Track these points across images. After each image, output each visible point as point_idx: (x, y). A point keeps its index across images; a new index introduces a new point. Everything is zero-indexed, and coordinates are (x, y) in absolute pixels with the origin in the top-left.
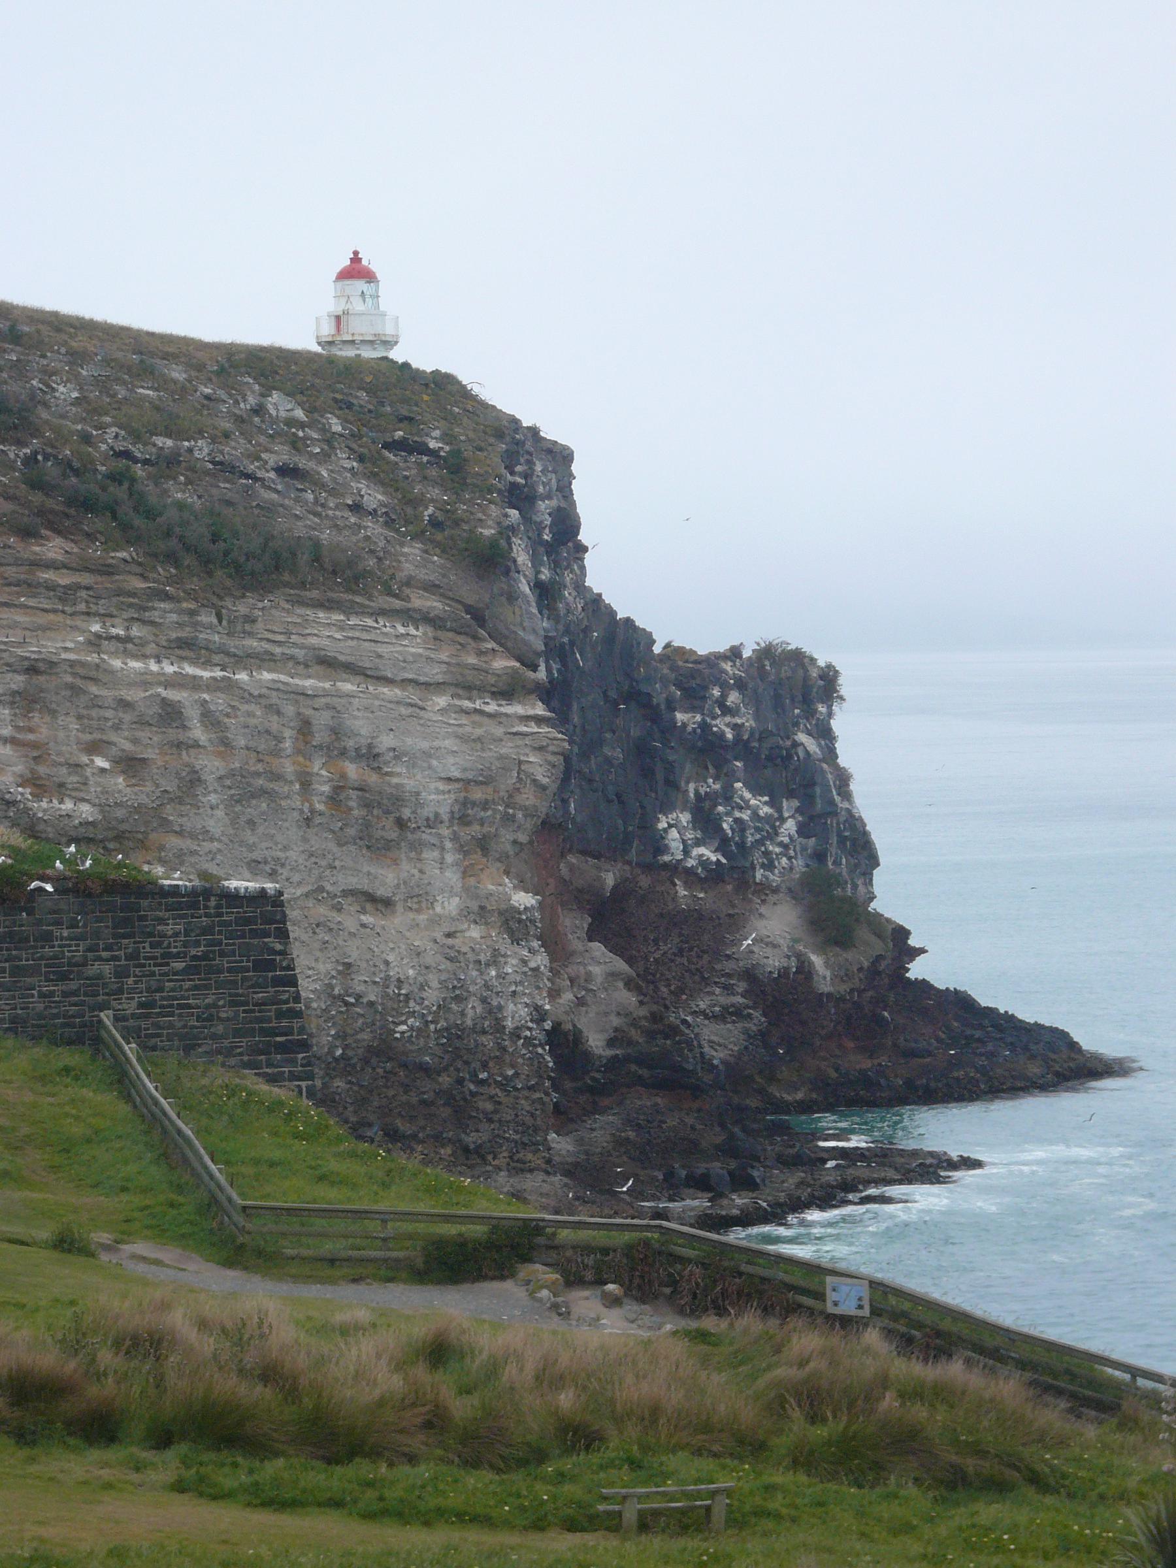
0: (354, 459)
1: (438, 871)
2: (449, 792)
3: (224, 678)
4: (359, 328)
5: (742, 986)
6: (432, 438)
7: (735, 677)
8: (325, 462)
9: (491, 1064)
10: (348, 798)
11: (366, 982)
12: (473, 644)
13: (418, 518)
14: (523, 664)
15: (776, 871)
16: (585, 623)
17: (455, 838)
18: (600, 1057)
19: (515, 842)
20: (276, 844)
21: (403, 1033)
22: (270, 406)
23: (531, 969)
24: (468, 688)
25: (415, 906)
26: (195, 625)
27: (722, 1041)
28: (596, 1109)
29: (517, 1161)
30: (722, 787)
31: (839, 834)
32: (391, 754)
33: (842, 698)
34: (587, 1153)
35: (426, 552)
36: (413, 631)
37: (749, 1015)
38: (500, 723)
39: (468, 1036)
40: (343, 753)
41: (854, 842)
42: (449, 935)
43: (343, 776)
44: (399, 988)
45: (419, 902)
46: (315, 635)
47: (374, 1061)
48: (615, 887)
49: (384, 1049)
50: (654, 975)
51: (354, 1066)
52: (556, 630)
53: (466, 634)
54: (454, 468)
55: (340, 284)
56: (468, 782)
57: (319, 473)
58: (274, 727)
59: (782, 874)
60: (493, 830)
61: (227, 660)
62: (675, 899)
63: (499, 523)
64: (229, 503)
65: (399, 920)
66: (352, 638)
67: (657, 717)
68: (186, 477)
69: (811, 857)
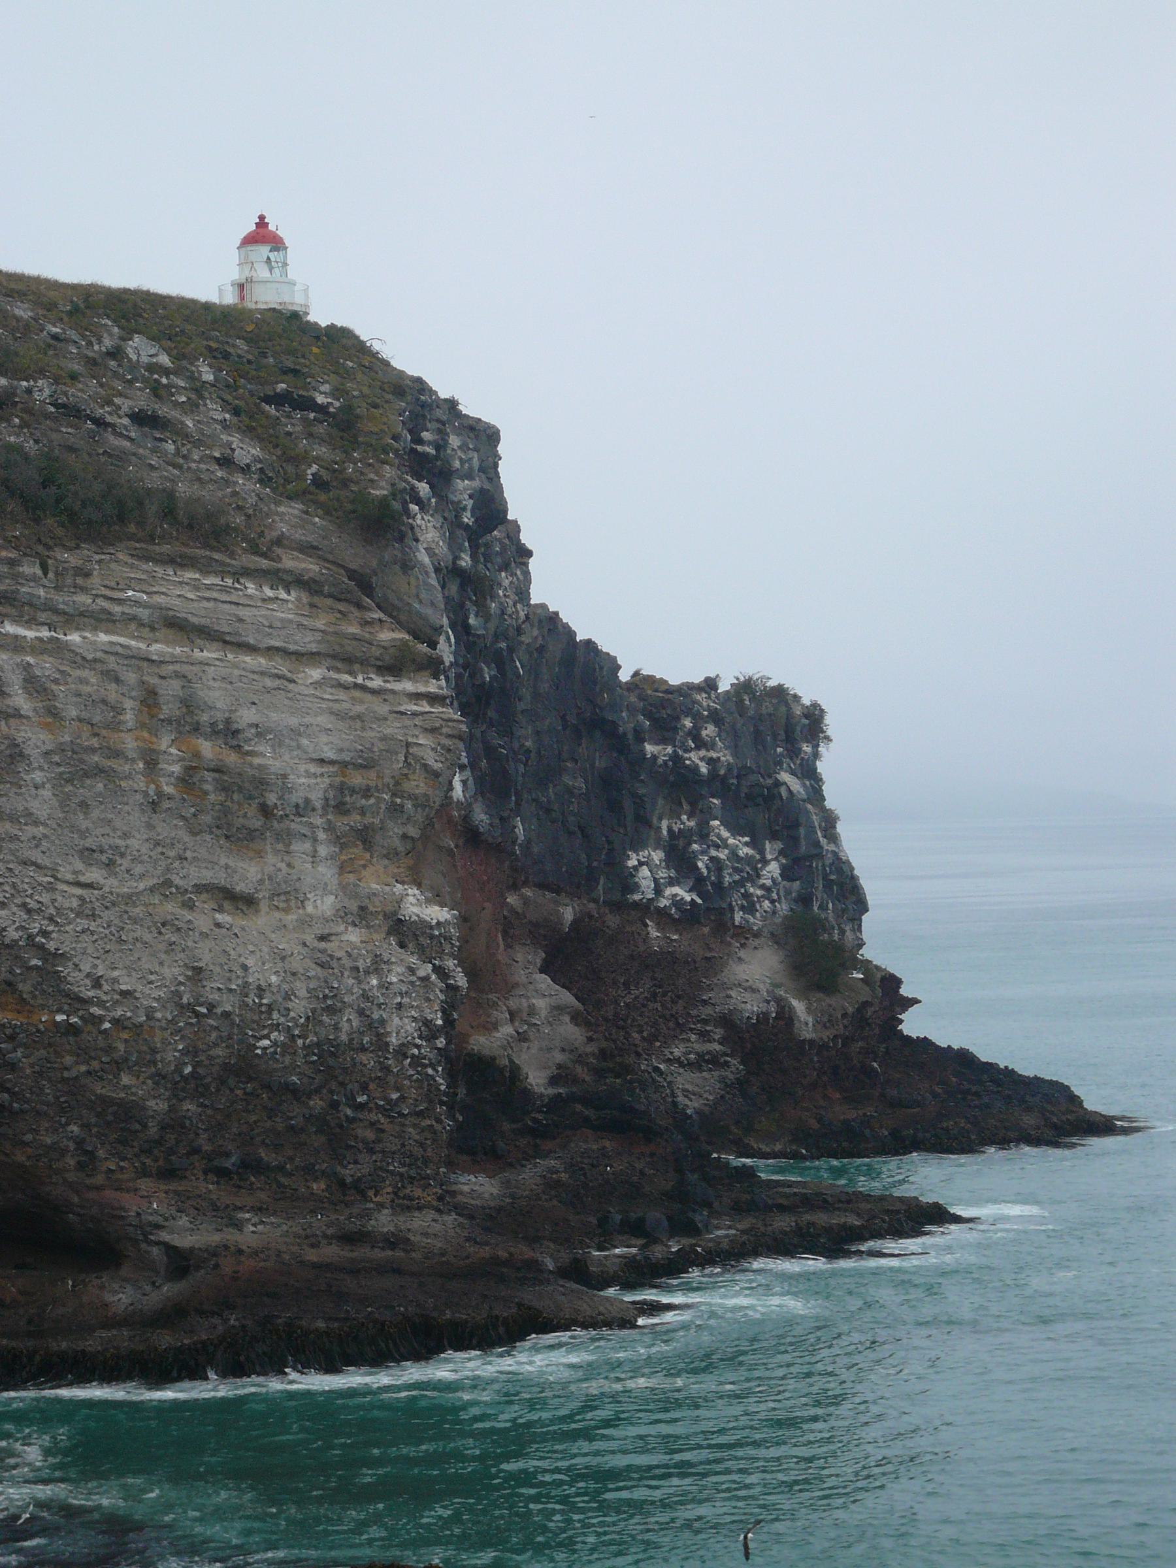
0: (228, 412)
1: (309, 866)
2: (322, 775)
3: (51, 639)
4: (265, 297)
5: (719, 1033)
6: (321, 393)
7: (709, 708)
8: (192, 412)
9: (372, 1086)
10: (203, 780)
11: (219, 989)
12: (357, 614)
13: (300, 477)
14: (416, 637)
15: (758, 914)
16: (540, 641)
17: (330, 828)
18: (542, 1095)
19: (405, 837)
20: (114, 830)
21: (265, 1049)
22: (130, 351)
23: (420, 978)
24: (348, 661)
25: (282, 905)
26: (16, 577)
27: (696, 1089)
28: (539, 1153)
29: (404, 1198)
30: (697, 824)
31: (825, 878)
32: (253, 731)
33: (828, 739)
34: (513, 1196)
35: (306, 513)
36: (283, 595)
37: (726, 1064)
38: (385, 700)
39: (344, 1053)
40: (196, 729)
41: (841, 886)
42: (322, 938)
43: (197, 755)
44: (261, 997)
45: (287, 901)
46: (163, 593)
47: (231, 1082)
48: (575, 922)
49: (244, 1067)
50: (625, 1021)
51: (206, 1087)
52: (485, 629)
53: (346, 600)
54: (345, 426)
56: (344, 765)
57: (182, 423)
58: (112, 697)
59: (764, 919)
60: (377, 821)
61: (55, 618)
62: (646, 939)
63: (393, 485)
64: (71, 449)
65: (263, 920)
66: (208, 599)
67: (622, 746)
68: (21, 419)
69: (796, 901)
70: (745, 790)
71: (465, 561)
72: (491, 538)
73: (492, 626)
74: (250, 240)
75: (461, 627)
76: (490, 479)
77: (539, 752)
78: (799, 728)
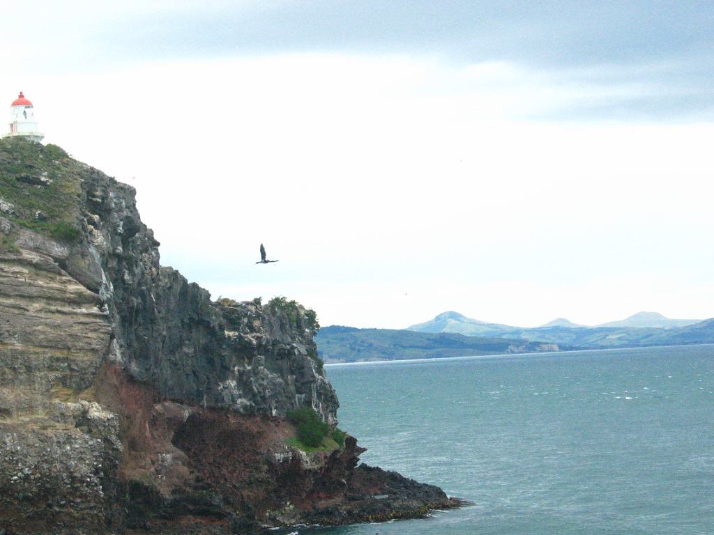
4: (22, 131)
6: (43, 176)
16: (169, 284)
21: (15, 480)
55: (13, 108)
70: (276, 352)
71: (120, 249)
72: (135, 239)
73: (136, 280)
74: (16, 104)
75: (118, 281)
76: (131, 212)
77: (170, 338)
78: (303, 321)
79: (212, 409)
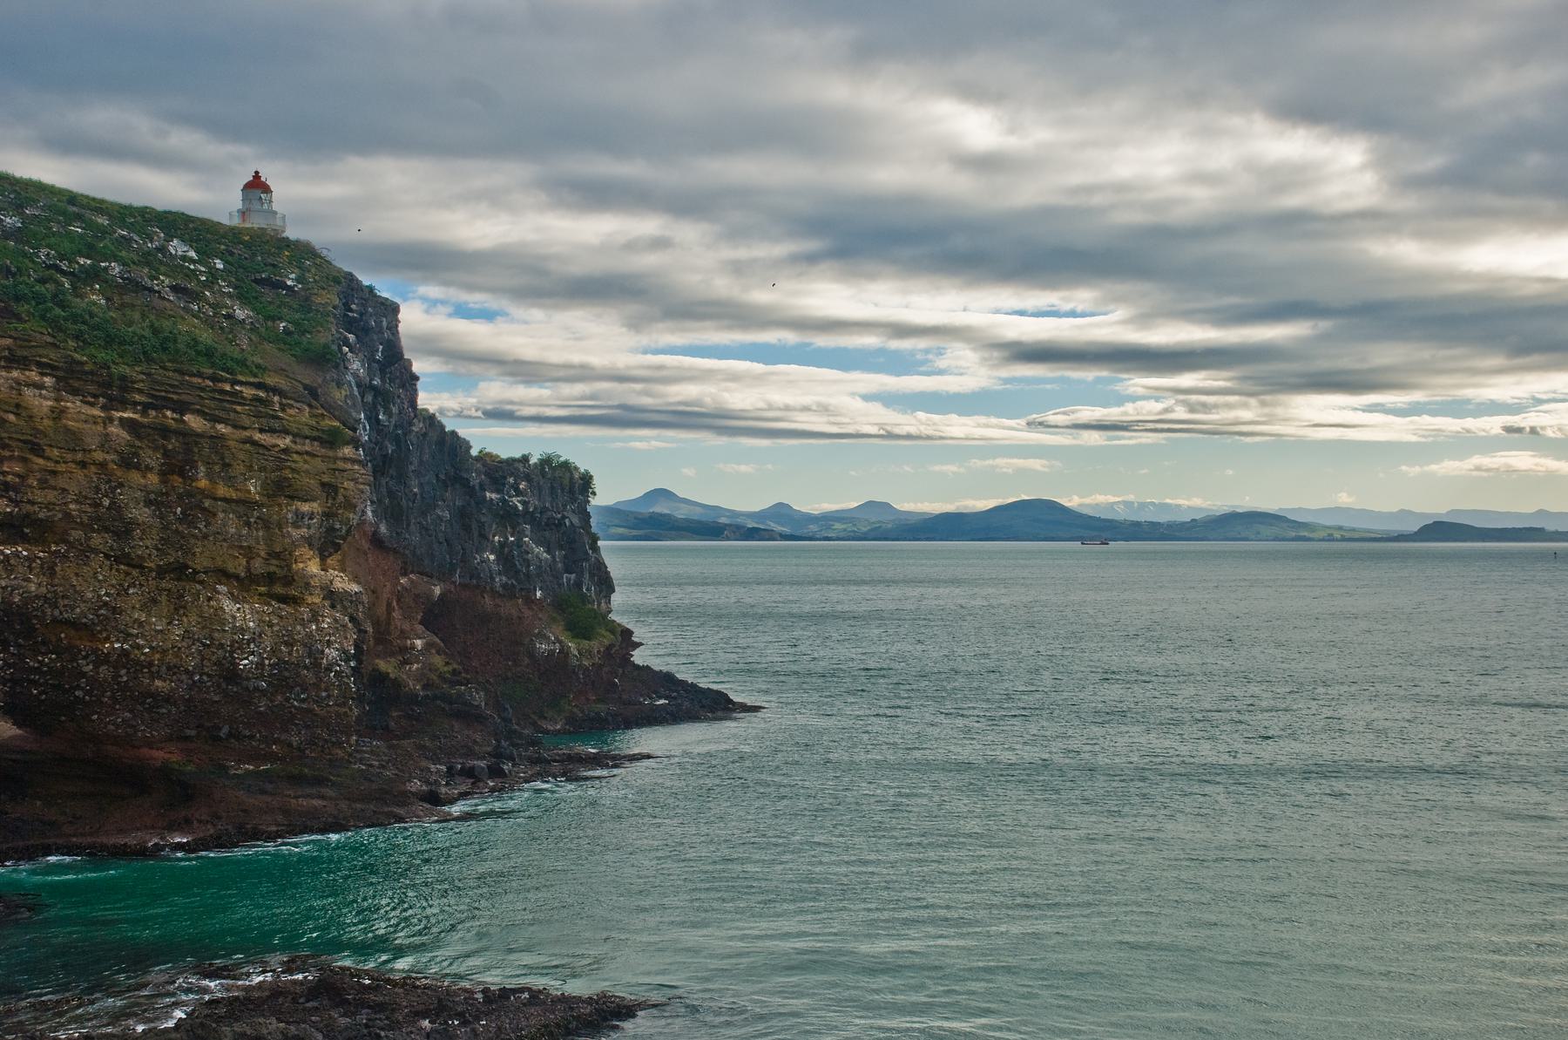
4: (256, 222)
74: (249, 187)
79: (464, 586)
